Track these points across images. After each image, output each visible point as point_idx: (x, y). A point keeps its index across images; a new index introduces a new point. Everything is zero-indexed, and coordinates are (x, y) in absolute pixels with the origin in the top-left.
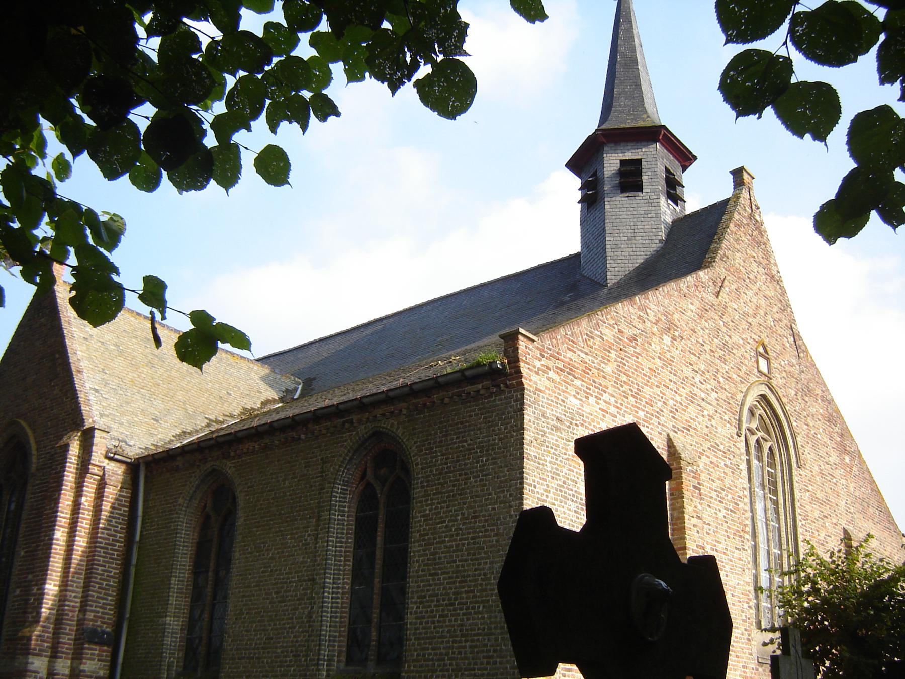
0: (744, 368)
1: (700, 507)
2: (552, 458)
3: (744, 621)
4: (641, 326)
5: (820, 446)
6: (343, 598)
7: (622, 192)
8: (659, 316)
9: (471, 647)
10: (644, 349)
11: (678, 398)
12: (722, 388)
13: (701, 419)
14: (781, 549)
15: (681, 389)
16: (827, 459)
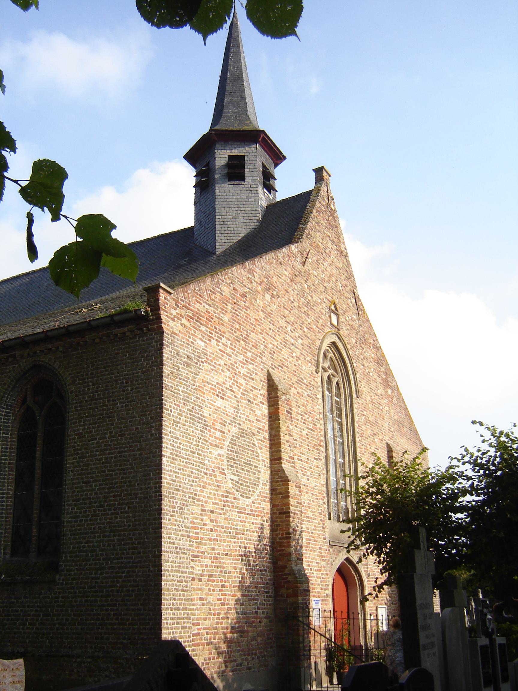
0: (321, 321)
1: (291, 427)
2: (184, 388)
3: (320, 514)
4: (249, 286)
5: (371, 382)
6: (7, 502)
7: (229, 180)
8: (263, 278)
9: (118, 540)
10: (252, 304)
11: (275, 343)
12: (306, 336)
13: (291, 359)
14: (344, 458)
15: (277, 336)
16: (376, 392)
